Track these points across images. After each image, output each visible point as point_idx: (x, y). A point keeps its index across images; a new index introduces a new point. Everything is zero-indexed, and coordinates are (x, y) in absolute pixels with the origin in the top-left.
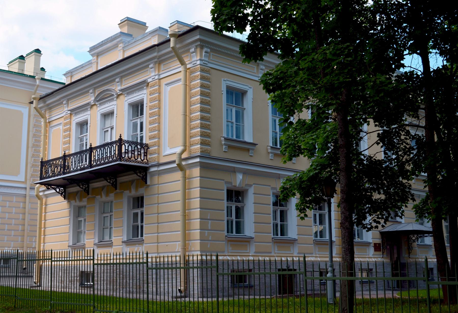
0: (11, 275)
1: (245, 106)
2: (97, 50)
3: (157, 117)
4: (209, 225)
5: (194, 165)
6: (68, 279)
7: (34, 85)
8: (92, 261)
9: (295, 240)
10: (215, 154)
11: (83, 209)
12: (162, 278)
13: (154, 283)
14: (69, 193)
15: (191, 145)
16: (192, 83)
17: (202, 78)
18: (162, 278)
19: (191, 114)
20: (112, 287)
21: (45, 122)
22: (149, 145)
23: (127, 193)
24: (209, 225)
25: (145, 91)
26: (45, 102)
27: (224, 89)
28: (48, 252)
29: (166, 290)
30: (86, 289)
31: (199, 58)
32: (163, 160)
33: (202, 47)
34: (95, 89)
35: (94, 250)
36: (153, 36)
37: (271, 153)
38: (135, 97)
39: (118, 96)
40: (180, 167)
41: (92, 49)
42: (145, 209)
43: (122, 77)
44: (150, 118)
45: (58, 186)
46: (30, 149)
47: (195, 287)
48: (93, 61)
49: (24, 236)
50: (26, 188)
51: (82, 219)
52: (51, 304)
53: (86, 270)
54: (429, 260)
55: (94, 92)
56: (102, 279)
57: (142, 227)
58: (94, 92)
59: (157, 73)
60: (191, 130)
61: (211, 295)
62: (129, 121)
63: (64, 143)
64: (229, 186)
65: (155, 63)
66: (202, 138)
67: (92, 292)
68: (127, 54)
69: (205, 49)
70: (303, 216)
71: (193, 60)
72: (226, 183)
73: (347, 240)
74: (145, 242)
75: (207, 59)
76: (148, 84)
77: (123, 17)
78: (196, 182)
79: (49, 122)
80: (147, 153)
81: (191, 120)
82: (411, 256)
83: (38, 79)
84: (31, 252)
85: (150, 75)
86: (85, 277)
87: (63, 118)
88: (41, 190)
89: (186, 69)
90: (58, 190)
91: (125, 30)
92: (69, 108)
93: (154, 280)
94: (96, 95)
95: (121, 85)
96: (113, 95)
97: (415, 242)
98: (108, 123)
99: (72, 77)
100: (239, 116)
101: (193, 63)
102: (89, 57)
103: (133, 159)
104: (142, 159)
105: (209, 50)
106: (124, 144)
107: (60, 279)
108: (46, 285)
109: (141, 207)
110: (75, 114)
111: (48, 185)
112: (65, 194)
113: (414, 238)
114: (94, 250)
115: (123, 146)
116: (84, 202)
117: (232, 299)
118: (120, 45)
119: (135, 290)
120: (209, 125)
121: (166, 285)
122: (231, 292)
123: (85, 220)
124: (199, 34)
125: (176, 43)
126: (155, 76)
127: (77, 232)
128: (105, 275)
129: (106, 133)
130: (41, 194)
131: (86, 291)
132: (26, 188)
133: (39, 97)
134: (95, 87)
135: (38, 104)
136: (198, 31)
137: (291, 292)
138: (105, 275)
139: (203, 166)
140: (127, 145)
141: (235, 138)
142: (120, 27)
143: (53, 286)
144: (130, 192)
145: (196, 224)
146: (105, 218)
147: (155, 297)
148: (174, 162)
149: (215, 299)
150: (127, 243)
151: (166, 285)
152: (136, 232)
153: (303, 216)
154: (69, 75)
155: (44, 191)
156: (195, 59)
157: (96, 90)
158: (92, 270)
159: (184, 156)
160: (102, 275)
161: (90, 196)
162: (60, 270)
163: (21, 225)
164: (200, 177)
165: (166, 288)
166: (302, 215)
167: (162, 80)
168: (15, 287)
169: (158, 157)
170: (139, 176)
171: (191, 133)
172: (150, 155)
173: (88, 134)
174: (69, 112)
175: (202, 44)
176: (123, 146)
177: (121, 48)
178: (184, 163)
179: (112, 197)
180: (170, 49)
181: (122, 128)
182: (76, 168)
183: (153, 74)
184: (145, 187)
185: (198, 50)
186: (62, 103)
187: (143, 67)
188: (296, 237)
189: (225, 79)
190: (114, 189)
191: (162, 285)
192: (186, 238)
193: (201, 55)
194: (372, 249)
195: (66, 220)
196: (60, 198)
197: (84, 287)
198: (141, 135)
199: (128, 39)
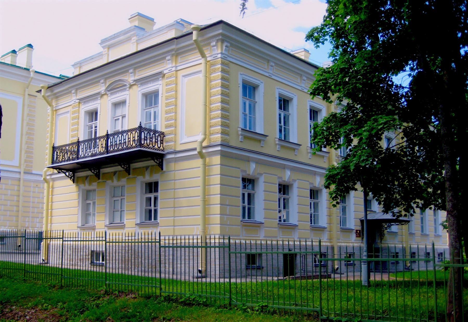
0: (33, 252)
1: (257, 99)
2: (108, 43)
3: (173, 107)
4: (228, 210)
5: (214, 153)
6: (76, 257)
7: (28, 77)
8: (158, 244)
9: (296, 226)
10: (232, 144)
11: (91, 194)
12: (179, 259)
13: (171, 264)
14: (78, 178)
15: (211, 134)
16: (212, 75)
17: (223, 71)
18: (179, 259)
19: (211, 105)
20: (123, 266)
21: (53, 111)
22: (165, 133)
23: (140, 178)
24: (228, 210)
25: (160, 82)
26: (52, 91)
27: (240, 82)
28: (59, 232)
29: (183, 270)
30: (98, 267)
31: (220, 51)
32: (179, 148)
33: (223, 41)
34: (106, 79)
35: (106, 233)
36: (170, 30)
37: (278, 144)
38: (150, 87)
39: (131, 86)
40: (201, 155)
41: (103, 42)
42: (160, 194)
43: (135, 69)
44: (166, 107)
45: (68, 170)
46: (24, 137)
47: (215, 267)
48: (104, 53)
49: (18, 216)
50: (20, 173)
51: (91, 202)
52: (106, 284)
53: (98, 250)
54: (427, 246)
55: (105, 82)
56: (114, 258)
57: (156, 211)
58: (105, 82)
59: (174, 65)
60: (211, 120)
61: (235, 275)
62: (143, 110)
63: (73, 130)
64: (244, 174)
65: (173, 55)
66: (223, 128)
67: (104, 271)
68: (141, 47)
69: (225, 44)
70: (335, 204)
71: (213, 53)
72: (242, 171)
73: (456, 228)
74: (160, 225)
75: (227, 53)
76: (164, 75)
77: (134, 11)
78: (217, 170)
79: (56, 110)
80: (163, 141)
81: (211, 111)
82: (383, 242)
83: (32, 71)
84: (31, 231)
85: (167, 66)
86: (95, 255)
87: (71, 107)
88: (48, 173)
89: (207, 62)
90: (67, 174)
91: (136, 23)
92: (78, 97)
93: (171, 261)
94: (107, 85)
95: (135, 75)
96: (126, 85)
97: (387, 229)
98: (119, 112)
99: (80, 67)
100: (252, 108)
101: (213, 56)
102: (100, 49)
103: (151, 146)
104: (159, 146)
105: (229, 45)
106: (143, 131)
107: (69, 257)
108: (54, 262)
109: (155, 192)
110: (84, 102)
111: (60, 169)
112: (74, 178)
113: (386, 226)
114: (106, 233)
115: (143, 133)
116: (94, 186)
117: (255, 280)
118: (133, 38)
119: (150, 270)
120: (228, 116)
121: (183, 265)
122: (244, 273)
123: (94, 203)
124: (222, 29)
125: (198, 36)
126: (172, 67)
127: (86, 213)
128: (117, 254)
129: (117, 122)
130: (48, 177)
131: (98, 269)
132: (20, 173)
133: (47, 86)
134: (106, 77)
135: (46, 93)
136: (221, 25)
137: (292, 273)
138: (117, 254)
139: (223, 155)
140: (146, 132)
141: (248, 129)
142: (131, 22)
143: (63, 264)
144: (144, 177)
145: (216, 209)
146: (123, 200)
147: (123, 272)
148: (195, 149)
149: (227, 280)
150: (140, 225)
151: (183, 265)
152: (150, 215)
153: (335, 204)
154: (78, 65)
155: (51, 175)
156: (216, 52)
157: (107, 81)
158: (104, 249)
159: (205, 144)
160: (114, 255)
161: (100, 180)
162: (69, 249)
163: (16, 206)
164: (221, 165)
165: (183, 268)
166: (334, 203)
167: (179, 72)
168: (24, 262)
169: (175, 145)
170: (156, 162)
171: (211, 123)
172: (166, 143)
173: (98, 121)
174: (78, 101)
175: (224, 39)
176: (143, 133)
177: (135, 41)
178: (204, 151)
179: (124, 181)
180: (191, 42)
181: (133, 117)
182: (86, 155)
183: (170, 66)
184: (160, 173)
185: (219, 44)
186: (70, 92)
187: (160, 59)
188: (297, 223)
189: (242, 73)
190: (127, 174)
191: (179, 265)
192: (206, 223)
193: (222, 49)
194: (354, 235)
195: (75, 203)
196: (69, 182)
197: (94, 265)
198: (155, 124)
199: (142, 33)
